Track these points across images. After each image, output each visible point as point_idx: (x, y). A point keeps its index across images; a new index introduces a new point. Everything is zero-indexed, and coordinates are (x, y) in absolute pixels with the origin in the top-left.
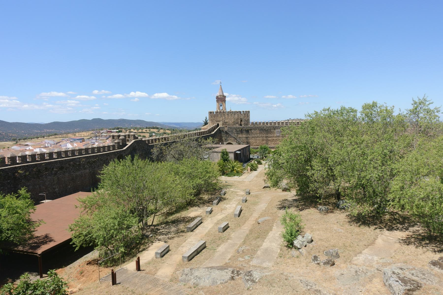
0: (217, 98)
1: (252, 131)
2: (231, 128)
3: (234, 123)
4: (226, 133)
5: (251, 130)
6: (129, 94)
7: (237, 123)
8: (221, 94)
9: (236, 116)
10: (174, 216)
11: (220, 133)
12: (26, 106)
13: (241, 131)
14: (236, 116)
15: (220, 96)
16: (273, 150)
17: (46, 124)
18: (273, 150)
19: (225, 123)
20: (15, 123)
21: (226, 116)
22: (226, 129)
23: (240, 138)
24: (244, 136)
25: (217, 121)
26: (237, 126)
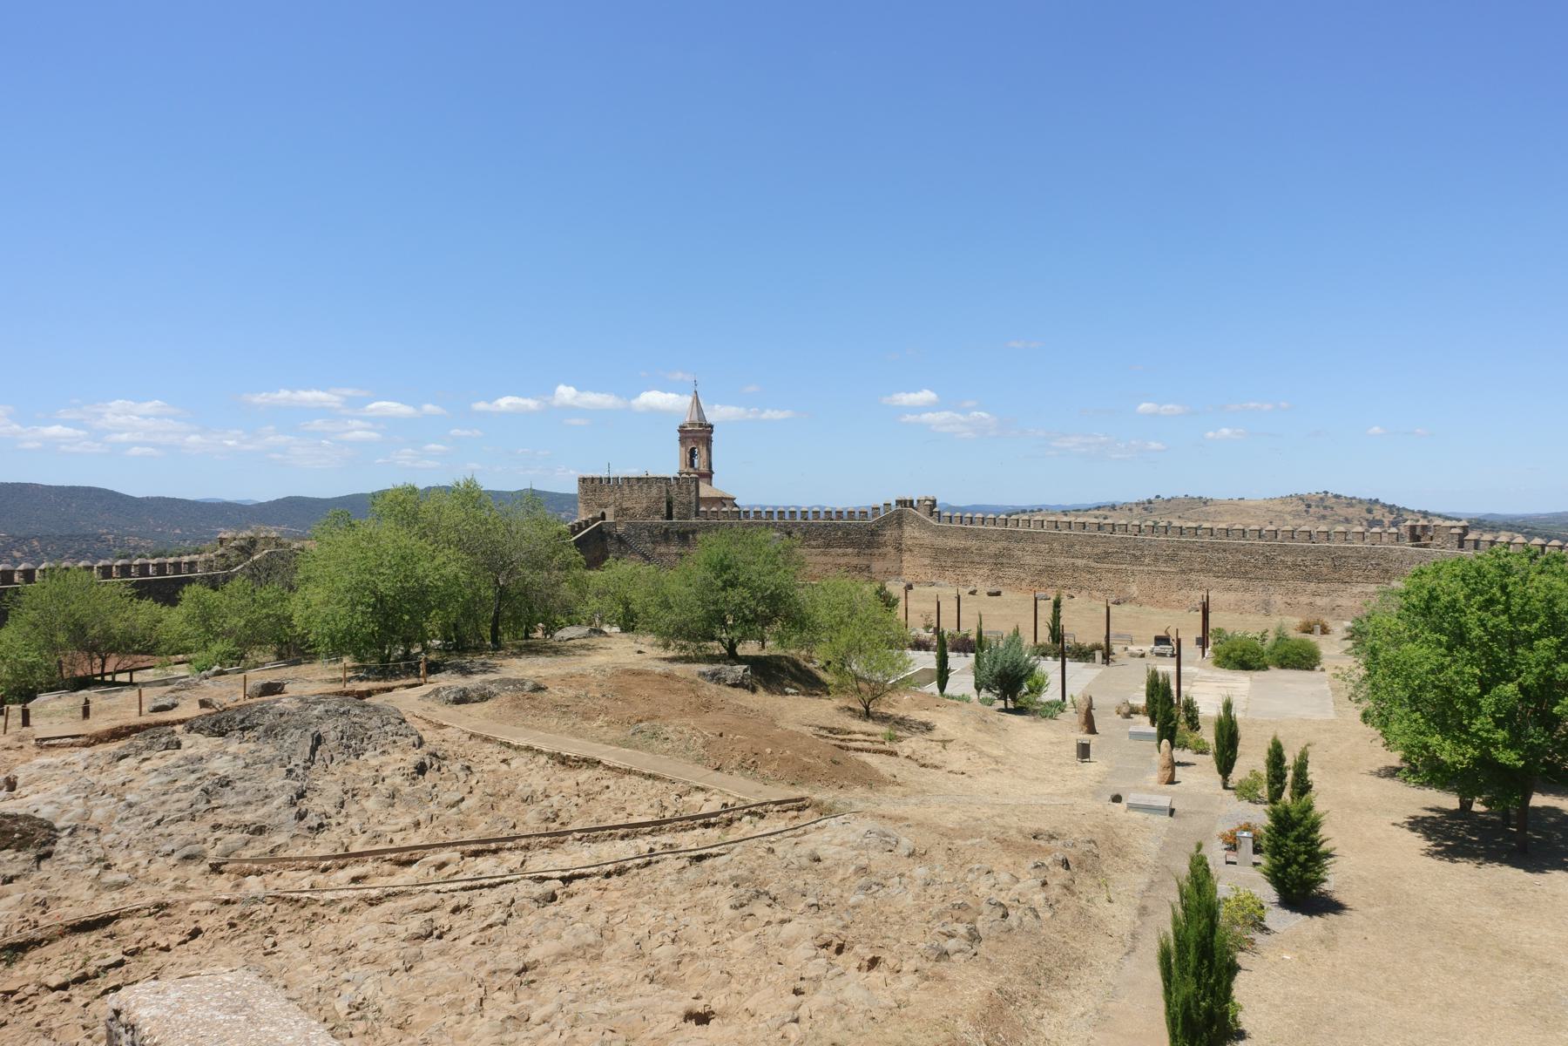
0: (682, 430)
1: (699, 537)
2: (634, 526)
3: (649, 511)
4: (620, 540)
5: (694, 532)
6: (637, 395)
7: (657, 512)
8: (695, 418)
9: (654, 491)
10: (1155, 797)
11: (603, 540)
12: (193, 438)
13: (666, 536)
14: (654, 491)
15: (693, 424)
16: (1289, 559)
17: (260, 504)
18: (1289, 559)
19: (621, 512)
20: (153, 499)
21: (627, 491)
22: (620, 529)
23: (661, 555)
24: (674, 549)
25: (600, 506)
26: (658, 519)
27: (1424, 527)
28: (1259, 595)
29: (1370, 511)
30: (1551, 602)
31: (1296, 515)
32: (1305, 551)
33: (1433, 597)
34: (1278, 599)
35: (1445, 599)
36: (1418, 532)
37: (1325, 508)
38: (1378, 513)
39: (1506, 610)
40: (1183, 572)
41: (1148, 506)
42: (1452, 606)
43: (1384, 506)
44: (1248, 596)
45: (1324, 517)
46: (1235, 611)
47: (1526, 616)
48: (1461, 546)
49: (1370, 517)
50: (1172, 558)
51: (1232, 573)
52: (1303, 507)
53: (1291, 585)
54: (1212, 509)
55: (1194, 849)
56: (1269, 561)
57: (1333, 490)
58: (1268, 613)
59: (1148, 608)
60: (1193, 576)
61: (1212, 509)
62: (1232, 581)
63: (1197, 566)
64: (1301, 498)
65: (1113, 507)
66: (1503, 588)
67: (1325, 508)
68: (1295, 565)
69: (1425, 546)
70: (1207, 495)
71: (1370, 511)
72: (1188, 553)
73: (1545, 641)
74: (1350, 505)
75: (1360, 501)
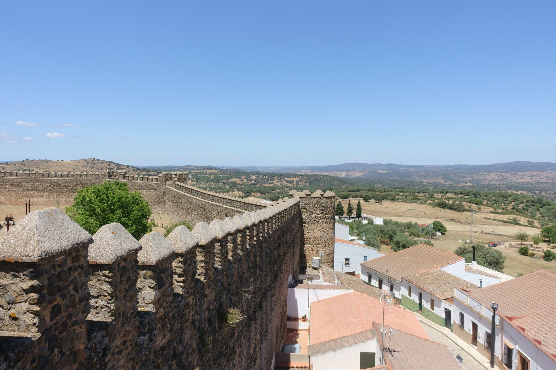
16: (66, 185)
27: (113, 172)
28: (54, 199)
29: (109, 165)
30: (120, 199)
31: (84, 167)
32: (72, 181)
33: (84, 199)
34: (62, 199)
35: (88, 199)
36: (111, 174)
37: (94, 164)
38: (112, 166)
39: (107, 202)
40: (24, 191)
41: (23, 163)
42: (90, 201)
43: (114, 163)
44: (50, 199)
45: (93, 167)
46: (46, 205)
47: (113, 204)
48: (124, 179)
49: (109, 167)
50: (19, 185)
51: (45, 191)
52: (86, 164)
53: (67, 194)
54: (50, 164)
55: (362, 261)
56: (59, 185)
57: (96, 158)
58: (58, 205)
59: (9, 206)
60: (28, 192)
61: (50, 164)
62: (44, 194)
63: (30, 188)
64: (85, 160)
65: (7, 164)
66: (107, 194)
67: (94, 164)
68: (68, 186)
69: (113, 179)
70: (48, 159)
71: (109, 165)
72: (25, 183)
73: (118, 211)
74: (103, 163)
75: (106, 162)
